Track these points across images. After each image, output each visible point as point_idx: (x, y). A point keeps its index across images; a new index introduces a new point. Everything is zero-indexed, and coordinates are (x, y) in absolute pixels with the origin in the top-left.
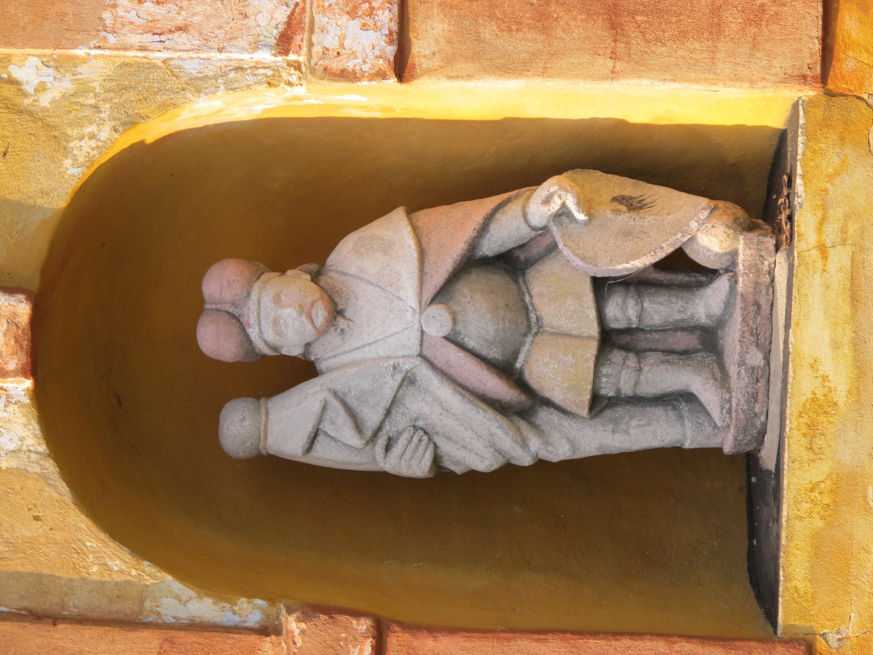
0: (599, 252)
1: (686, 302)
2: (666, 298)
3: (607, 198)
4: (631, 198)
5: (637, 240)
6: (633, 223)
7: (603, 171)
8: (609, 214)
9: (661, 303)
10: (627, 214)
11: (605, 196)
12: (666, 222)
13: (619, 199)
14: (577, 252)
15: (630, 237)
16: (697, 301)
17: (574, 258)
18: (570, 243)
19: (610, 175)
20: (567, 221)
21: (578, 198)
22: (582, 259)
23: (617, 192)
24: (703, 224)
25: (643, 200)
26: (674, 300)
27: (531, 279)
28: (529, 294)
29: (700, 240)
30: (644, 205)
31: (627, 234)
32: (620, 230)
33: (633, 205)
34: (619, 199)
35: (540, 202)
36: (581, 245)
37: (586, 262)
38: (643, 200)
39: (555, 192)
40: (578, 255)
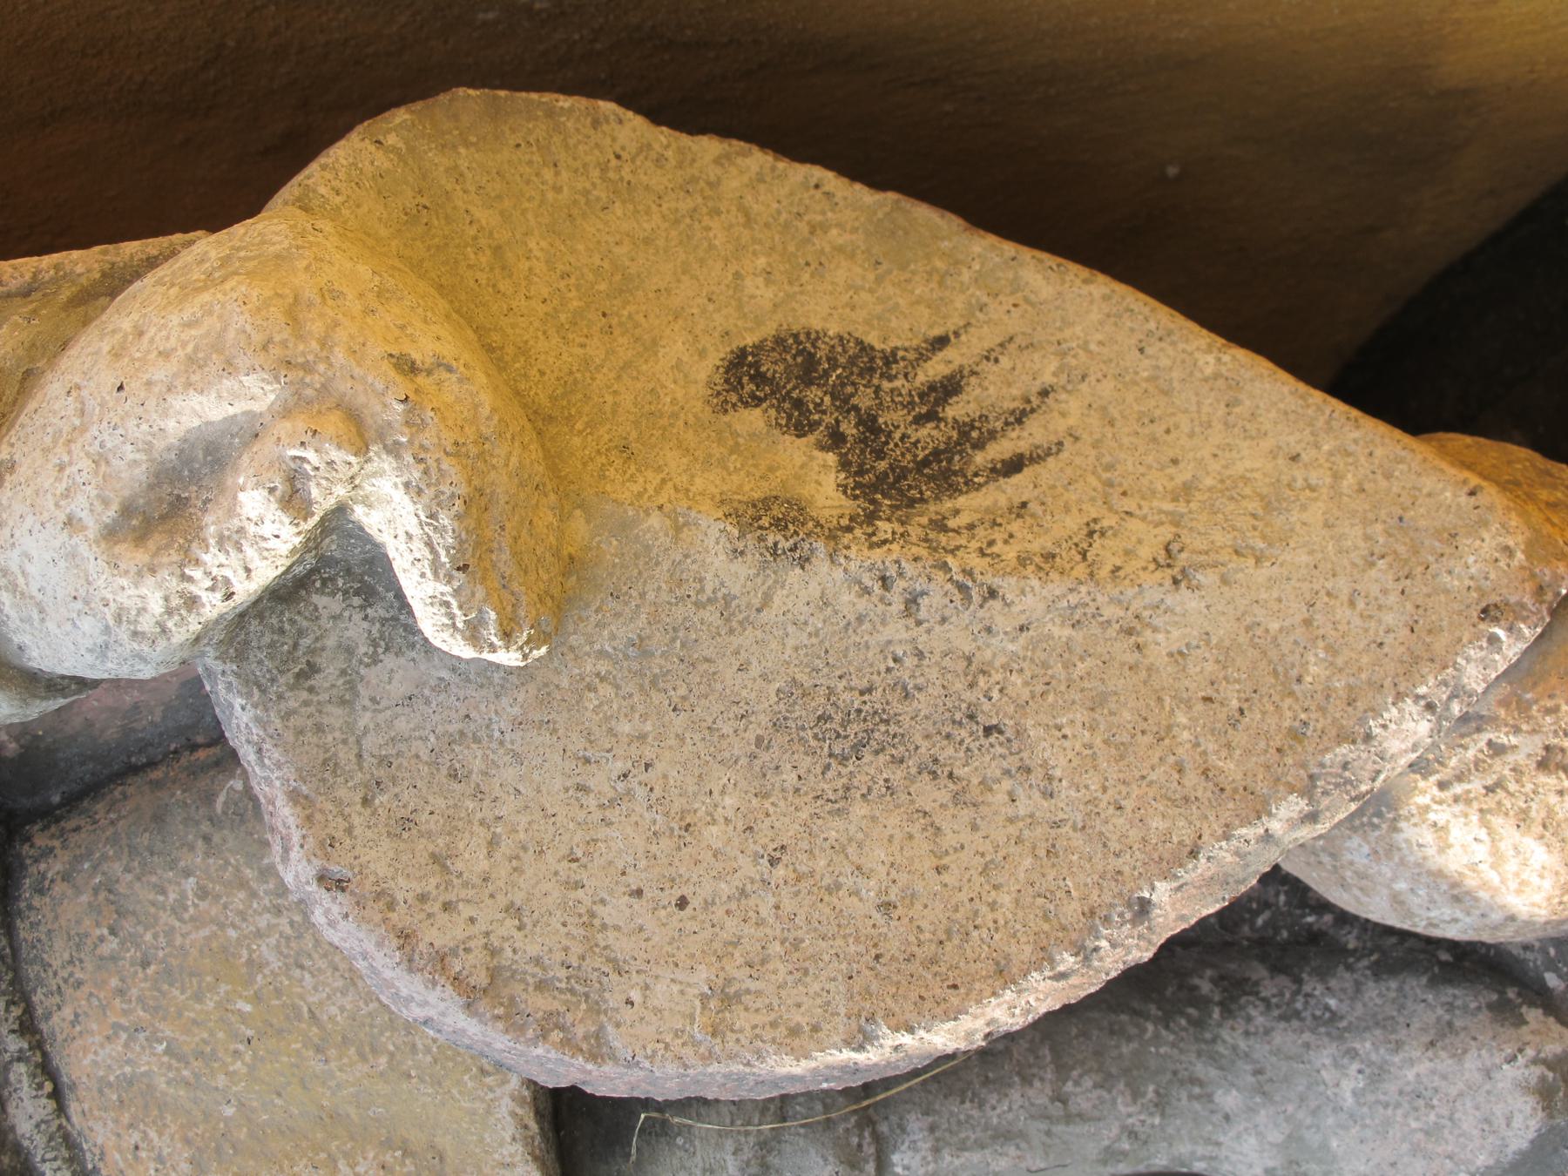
0: (616, 910)
1: (1161, 1104)
2: (1039, 1094)
3: (687, 365)
4: (871, 363)
5: (931, 794)
6: (897, 631)
7: (656, 116)
8: (717, 557)
9: (1004, 1136)
10: (859, 558)
11: (676, 347)
12: (1161, 644)
13: (781, 377)
14: (438, 934)
15: (872, 766)
16: (1229, 1100)
17: (409, 985)
18: (376, 857)
19: (708, 147)
20: (356, 629)
21: (476, 504)
22: (471, 996)
23: (763, 307)
24: (1471, 722)
25: (949, 388)
26: (1083, 1093)
27: (59, 954)
28: (47, 1070)
29: (1415, 834)
30: (971, 435)
31: (850, 730)
32: (794, 691)
33: (894, 445)
34: (781, 377)
35: (93, 515)
36: (472, 858)
37: (513, 1019)
38: (949, 388)
39: (251, 431)
40: (441, 959)
